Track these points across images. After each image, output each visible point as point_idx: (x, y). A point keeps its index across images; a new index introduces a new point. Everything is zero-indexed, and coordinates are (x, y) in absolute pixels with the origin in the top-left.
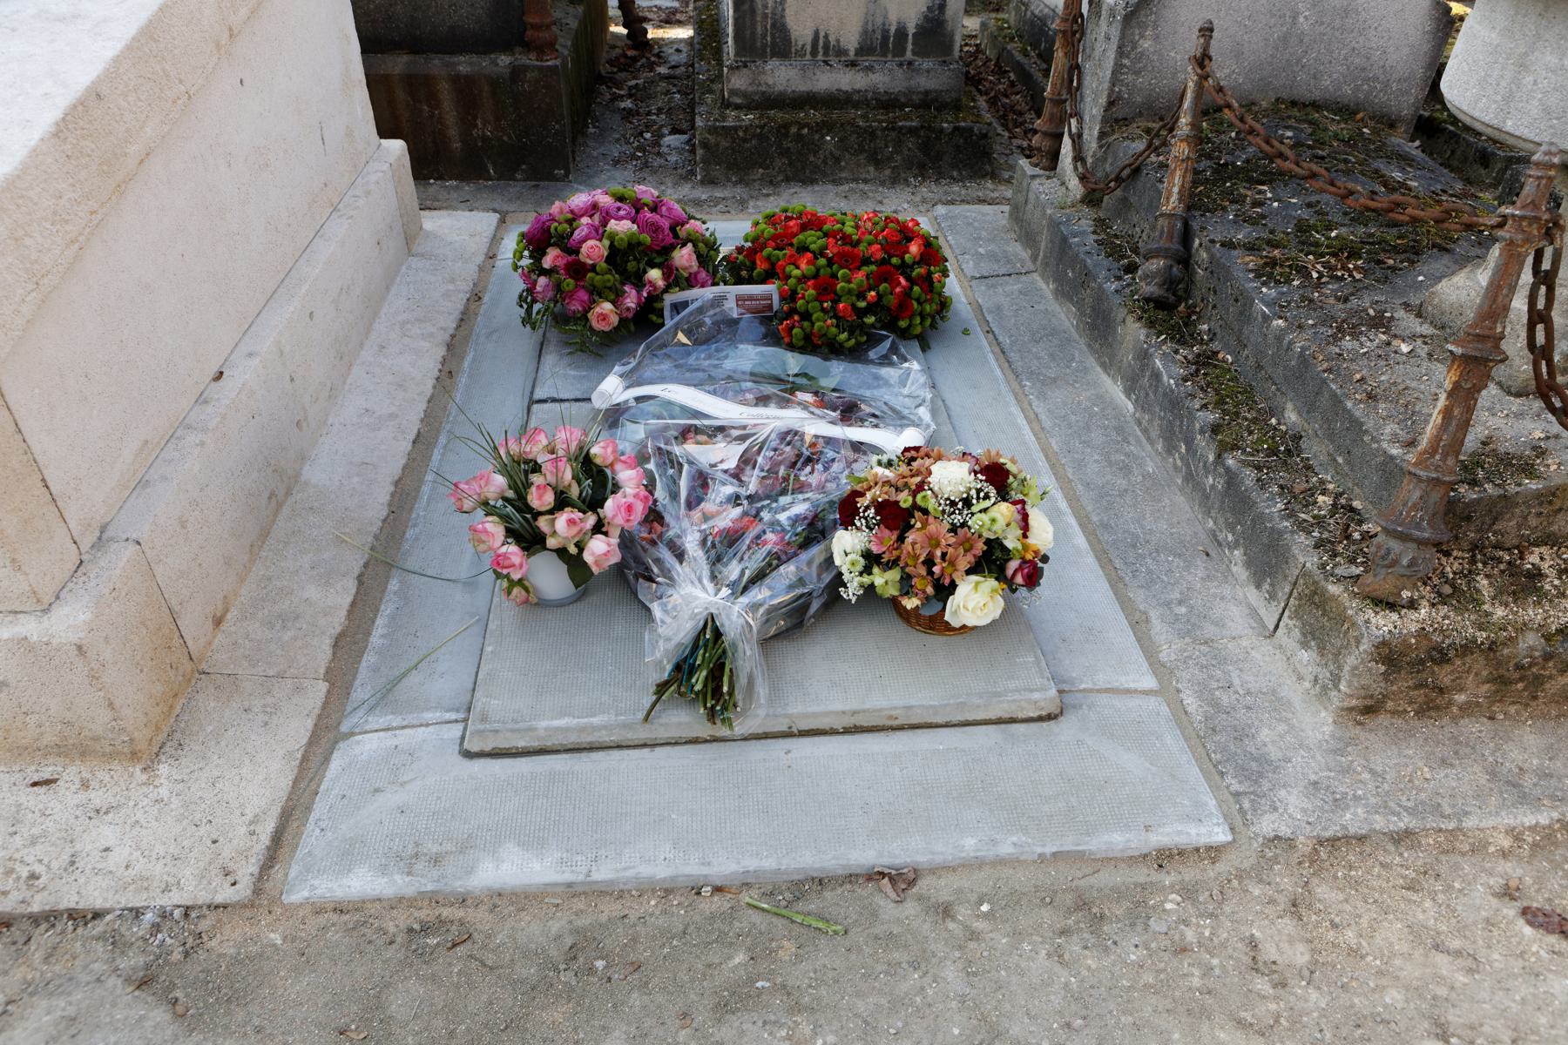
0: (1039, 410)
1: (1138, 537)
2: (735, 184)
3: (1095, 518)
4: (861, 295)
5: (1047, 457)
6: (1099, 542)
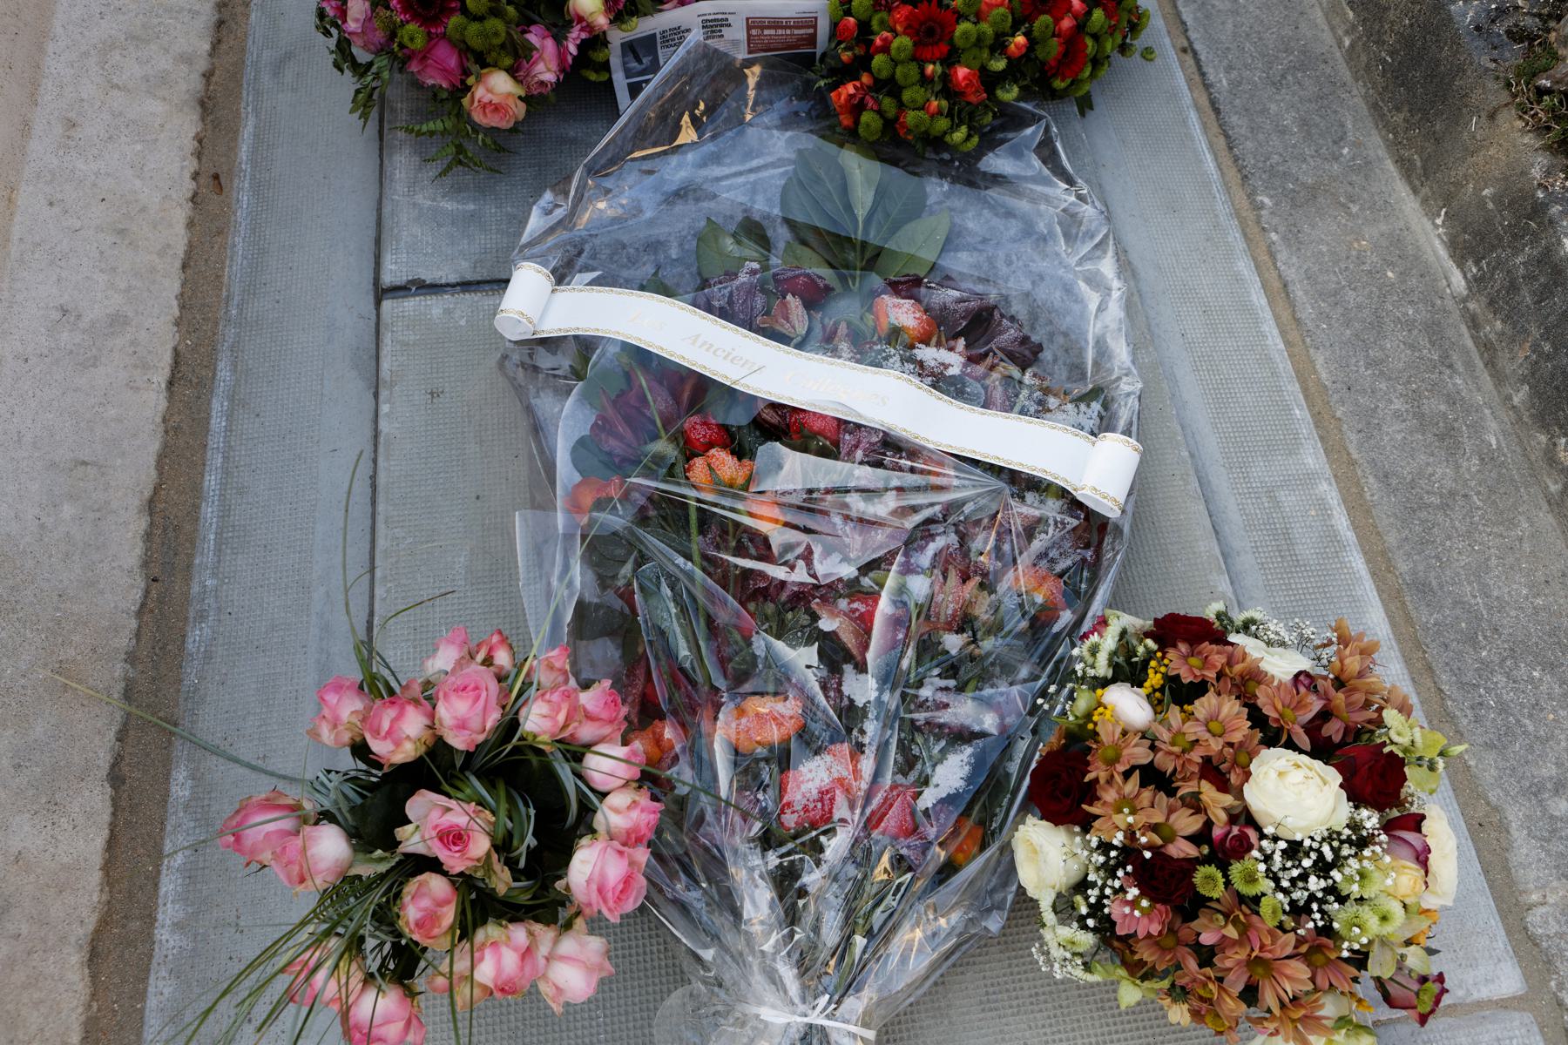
0: (1291, 274)
1: (1479, 618)
3: (1403, 567)
4: (999, 45)
5: (1305, 391)
6: (1409, 620)
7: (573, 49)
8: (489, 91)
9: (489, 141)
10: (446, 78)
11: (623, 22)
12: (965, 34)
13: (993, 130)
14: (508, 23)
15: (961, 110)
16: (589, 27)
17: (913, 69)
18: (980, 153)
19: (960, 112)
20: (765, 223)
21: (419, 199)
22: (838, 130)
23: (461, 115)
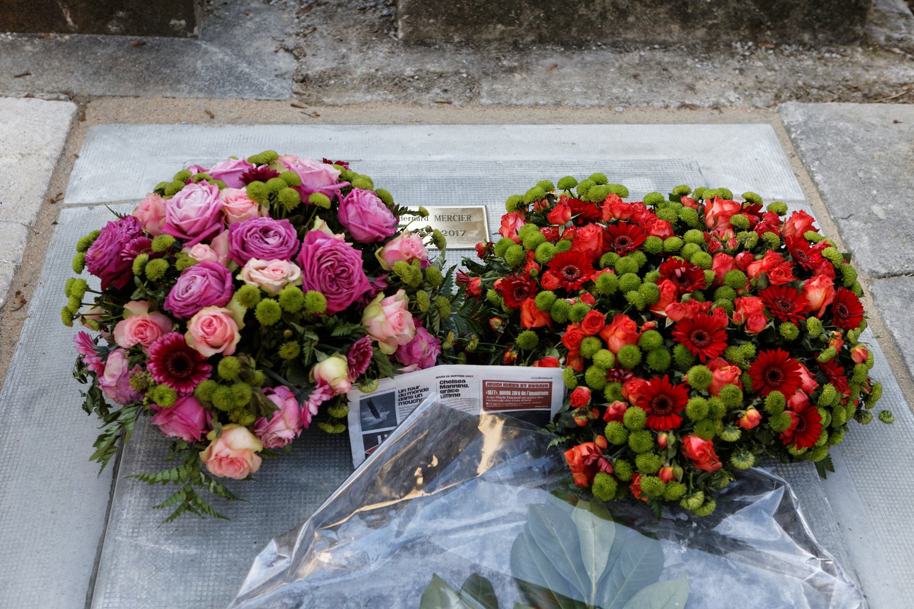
2: (459, 47)
4: (731, 418)
7: (313, 410)
8: (228, 446)
9: (220, 489)
10: (188, 432)
11: (363, 384)
12: (697, 408)
13: (731, 492)
14: (254, 386)
15: (695, 478)
16: (332, 390)
17: (646, 439)
18: (716, 518)
19: (695, 478)
20: (494, 582)
21: (142, 540)
22: (571, 486)
23: (196, 464)
